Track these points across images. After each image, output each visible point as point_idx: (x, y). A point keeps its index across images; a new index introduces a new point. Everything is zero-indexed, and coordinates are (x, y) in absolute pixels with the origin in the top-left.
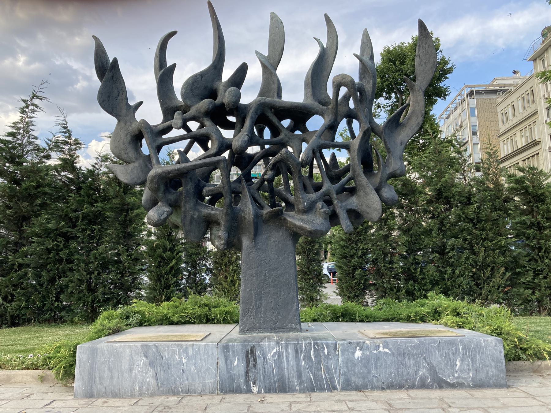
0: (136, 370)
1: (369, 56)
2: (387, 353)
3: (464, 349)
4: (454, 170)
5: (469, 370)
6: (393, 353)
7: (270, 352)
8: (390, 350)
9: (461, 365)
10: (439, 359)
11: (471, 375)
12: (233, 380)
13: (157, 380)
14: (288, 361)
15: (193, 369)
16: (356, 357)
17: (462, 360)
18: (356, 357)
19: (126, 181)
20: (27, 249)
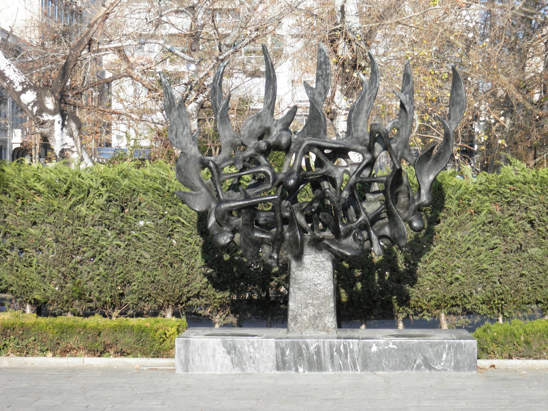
0: (218, 356)
1: (83, 127)
2: (395, 348)
3: (449, 347)
4: (472, 146)
5: (451, 360)
6: (398, 348)
7: (312, 345)
8: (397, 346)
9: (446, 357)
10: (432, 353)
11: (452, 364)
12: (172, 349)
13: (232, 362)
14: (324, 353)
15: (257, 356)
16: (373, 350)
17: (447, 354)
18: (373, 350)
19: (148, 145)
20: (500, 113)
